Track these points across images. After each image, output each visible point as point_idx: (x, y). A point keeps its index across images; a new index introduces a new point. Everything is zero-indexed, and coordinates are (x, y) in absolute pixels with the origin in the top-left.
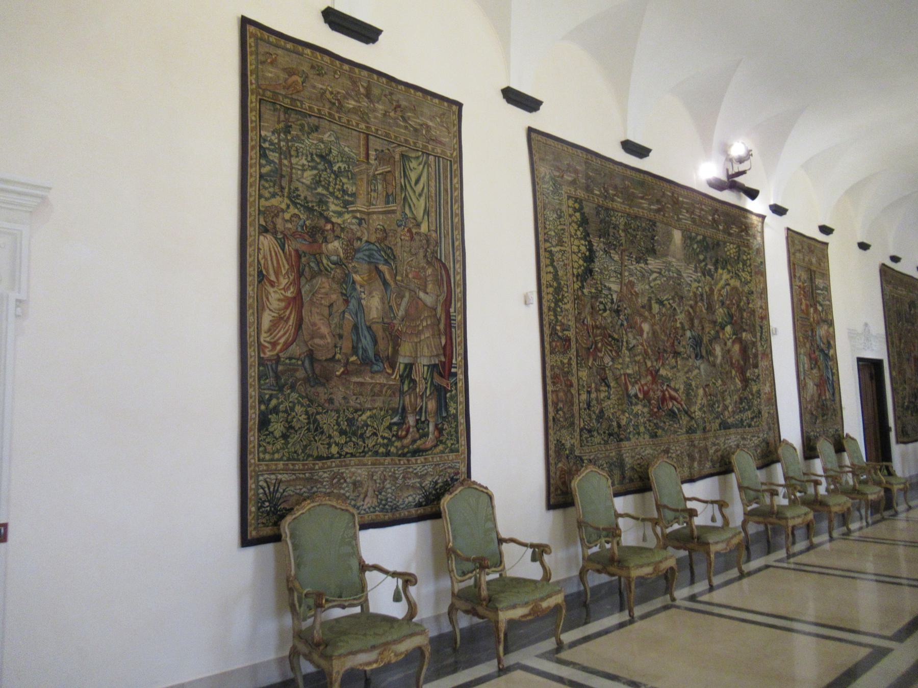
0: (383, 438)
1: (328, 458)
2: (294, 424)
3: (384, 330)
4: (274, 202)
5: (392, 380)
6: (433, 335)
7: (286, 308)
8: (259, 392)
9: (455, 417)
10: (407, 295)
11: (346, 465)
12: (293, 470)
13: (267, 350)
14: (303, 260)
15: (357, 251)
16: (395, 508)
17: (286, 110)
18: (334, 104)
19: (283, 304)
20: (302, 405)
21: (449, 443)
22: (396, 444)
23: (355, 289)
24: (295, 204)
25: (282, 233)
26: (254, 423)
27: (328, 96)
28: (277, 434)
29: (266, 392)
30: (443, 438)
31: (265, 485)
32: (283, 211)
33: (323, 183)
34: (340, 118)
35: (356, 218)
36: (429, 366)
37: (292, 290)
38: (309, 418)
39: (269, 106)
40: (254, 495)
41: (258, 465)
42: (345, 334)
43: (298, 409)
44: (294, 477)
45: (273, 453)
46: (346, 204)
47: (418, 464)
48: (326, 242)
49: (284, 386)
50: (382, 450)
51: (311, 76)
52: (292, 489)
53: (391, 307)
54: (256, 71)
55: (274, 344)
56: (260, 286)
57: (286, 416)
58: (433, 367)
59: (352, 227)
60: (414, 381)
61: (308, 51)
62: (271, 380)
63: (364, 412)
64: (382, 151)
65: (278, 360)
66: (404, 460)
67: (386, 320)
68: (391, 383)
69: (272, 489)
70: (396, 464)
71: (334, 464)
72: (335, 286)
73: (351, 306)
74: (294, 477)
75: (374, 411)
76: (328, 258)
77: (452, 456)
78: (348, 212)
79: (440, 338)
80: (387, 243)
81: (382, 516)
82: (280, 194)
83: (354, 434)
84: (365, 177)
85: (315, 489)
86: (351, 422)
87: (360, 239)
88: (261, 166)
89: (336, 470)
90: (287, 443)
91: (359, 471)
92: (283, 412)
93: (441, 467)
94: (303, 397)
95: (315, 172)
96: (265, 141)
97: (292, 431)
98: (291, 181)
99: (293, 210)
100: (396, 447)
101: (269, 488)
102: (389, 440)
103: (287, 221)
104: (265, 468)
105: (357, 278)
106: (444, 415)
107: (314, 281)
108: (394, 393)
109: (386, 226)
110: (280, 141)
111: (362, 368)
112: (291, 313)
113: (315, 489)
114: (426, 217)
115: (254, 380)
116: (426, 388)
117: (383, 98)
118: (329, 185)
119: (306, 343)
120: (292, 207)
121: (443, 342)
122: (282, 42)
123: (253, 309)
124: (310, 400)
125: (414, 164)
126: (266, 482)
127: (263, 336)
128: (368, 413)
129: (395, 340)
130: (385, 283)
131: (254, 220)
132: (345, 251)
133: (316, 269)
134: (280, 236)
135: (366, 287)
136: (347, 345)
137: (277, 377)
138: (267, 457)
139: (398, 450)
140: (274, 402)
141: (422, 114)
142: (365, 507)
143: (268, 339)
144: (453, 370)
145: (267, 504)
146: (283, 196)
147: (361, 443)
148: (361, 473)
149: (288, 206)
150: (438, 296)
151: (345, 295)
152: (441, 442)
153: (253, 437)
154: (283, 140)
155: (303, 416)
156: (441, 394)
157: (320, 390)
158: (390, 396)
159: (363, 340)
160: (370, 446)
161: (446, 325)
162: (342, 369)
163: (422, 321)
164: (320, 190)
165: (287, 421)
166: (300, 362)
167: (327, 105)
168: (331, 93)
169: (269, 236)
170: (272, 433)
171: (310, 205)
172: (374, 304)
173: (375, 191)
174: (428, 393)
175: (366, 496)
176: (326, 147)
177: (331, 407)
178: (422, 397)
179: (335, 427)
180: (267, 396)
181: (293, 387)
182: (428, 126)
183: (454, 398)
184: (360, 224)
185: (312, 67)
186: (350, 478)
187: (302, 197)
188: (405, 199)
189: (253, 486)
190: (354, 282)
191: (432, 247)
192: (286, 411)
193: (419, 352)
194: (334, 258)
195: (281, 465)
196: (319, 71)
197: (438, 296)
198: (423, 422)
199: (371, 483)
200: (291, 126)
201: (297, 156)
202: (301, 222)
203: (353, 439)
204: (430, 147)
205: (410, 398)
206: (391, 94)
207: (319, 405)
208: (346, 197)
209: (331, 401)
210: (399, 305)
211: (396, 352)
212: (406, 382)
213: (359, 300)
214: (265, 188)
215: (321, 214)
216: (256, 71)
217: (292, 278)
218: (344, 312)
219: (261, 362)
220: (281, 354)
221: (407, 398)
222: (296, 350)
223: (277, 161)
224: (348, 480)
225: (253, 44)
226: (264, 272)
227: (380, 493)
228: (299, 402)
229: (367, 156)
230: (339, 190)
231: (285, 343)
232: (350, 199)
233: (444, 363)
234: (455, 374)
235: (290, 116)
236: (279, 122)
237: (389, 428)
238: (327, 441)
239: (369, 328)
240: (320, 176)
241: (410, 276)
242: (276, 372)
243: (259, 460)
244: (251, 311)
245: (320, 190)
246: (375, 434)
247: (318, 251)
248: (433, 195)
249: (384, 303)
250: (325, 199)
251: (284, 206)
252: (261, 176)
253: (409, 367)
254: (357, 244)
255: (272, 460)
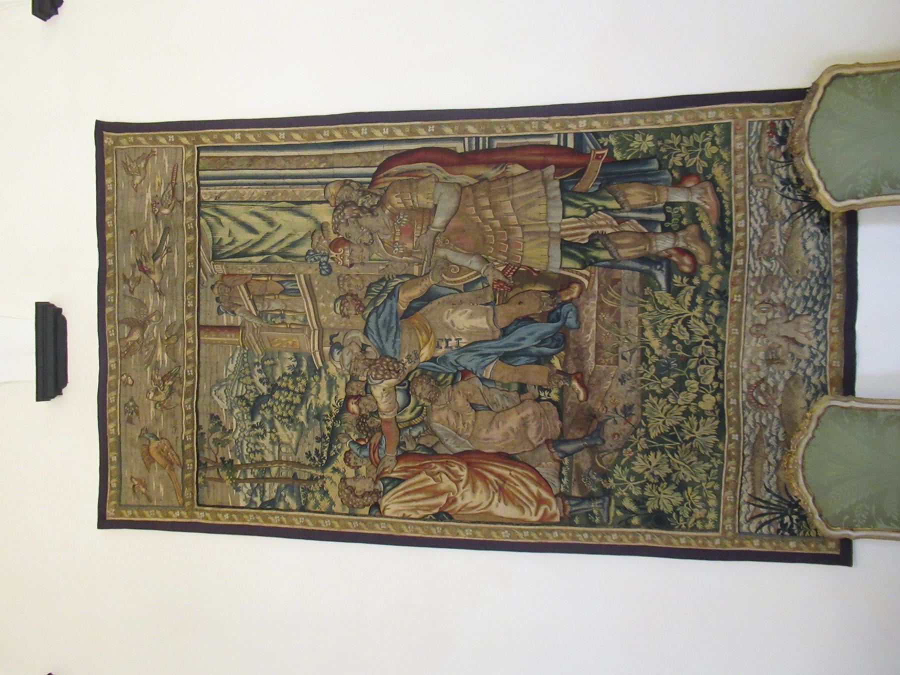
0: (693, 305)
1: (721, 416)
2: (662, 475)
3: (506, 301)
4: (333, 492)
5: (591, 286)
6: (509, 192)
7: (484, 479)
8: (613, 526)
9: (661, 135)
10: (442, 252)
11: (736, 378)
12: (737, 475)
13: (550, 512)
14: (410, 447)
15: (383, 354)
16: (824, 280)
17: (202, 465)
18: (171, 387)
19: (479, 484)
20: (633, 458)
21: (710, 150)
22: (705, 276)
23: (444, 359)
24: (331, 459)
25: (375, 483)
26: (659, 535)
27: (162, 397)
28: (677, 499)
29: (612, 515)
30: (702, 165)
31: (755, 523)
32: (344, 479)
33: (291, 413)
34: (188, 378)
35: (331, 353)
36: (565, 203)
37: (456, 468)
38: (655, 450)
39: (204, 491)
40: (770, 541)
41: (725, 532)
42: (517, 377)
43: (639, 466)
44: (748, 474)
45: (708, 508)
46: (314, 371)
47: (747, 225)
48: (377, 412)
49: (604, 489)
50: (714, 310)
51: (143, 425)
52: (767, 477)
53: (468, 287)
54: (165, 509)
55: (540, 501)
56: (455, 517)
57: (649, 486)
58: (568, 195)
59: (346, 362)
60: (593, 238)
61: (110, 427)
62: (595, 506)
63: (646, 345)
64: (217, 299)
65: (563, 496)
66: (737, 259)
67: (490, 299)
68: (596, 287)
69: (764, 511)
70: (743, 274)
71: (733, 366)
72: (443, 398)
73: (471, 366)
74: (748, 474)
75: (646, 322)
76: (401, 410)
77: (737, 142)
78: (326, 367)
79: (513, 177)
80: (361, 295)
81: (836, 307)
82: (320, 482)
83: (683, 363)
84: (265, 333)
85: (772, 441)
86: (662, 370)
87: (363, 348)
88: (288, 509)
89: (742, 398)
90: (693, 484)
91: (748, 352)
92: (643, 490)
93: (756, 170)
94: (621, 457)
95: (277, 423)
96: (251, 501)
97: (674, 476)
98: (299, 464)
99: (339, 463)
100: (711, 275)
101: (762, 515)
102: (696, 292)
103: (357, 474)
104: (729, 520)
105: (425, 354)
106: (655, 165)
107: (439, 432)
108: (616, 281)
109: (335, 296)
110: (246, 480)
111: (572, 346)
112: (492, 472)
113: (772, 441)
114: (306, 208)
115: (595, 533)
116: (606, 210)
117: (136, 295)
118: (291, 403)
119: (536, 449)
120: (335, 465)
121: (517, 169)
122: (112, 468)
123: (490, 529)
124: (626, 446)
125: (222, 234)
126: (753, 518)
127: (529, 516)
128: (649, 334)
129: (522, 276)
130: (428, 297)
131: (365, 522)
132: (388, 374)
133: (420, 429)
134: (380, 486)
135: (439, 336)
136: (536, 375)
137: (590, 497)
138: (712, 515)
139: (717, 272)
140: (628, 504)
141: (139, 215)
142: (813, 343)
143: (533, 509)
144: (571, 144)
145: (787, 519)
146: (322, 477)
147: (700, 350)
148: (752, 349)
149: (336, 470)
150: (437, 181)
151: (455, 375)
152: (707, 171)
153: (681, 539)
154: (245, 472)
155: (651, 457)
156: (620, 172)
157: (609, 429)
158: (619, 291)
159: (525, 344)
160: (705, 331)
161: (488, 164)
162: (575, 384)
163: (485, 220)
164: (302, 418)
165: (658, 484)
166: (566, 461)
167: (175, 399)
168: (156, 392)
169: (383, 503)
170: (675, 508)
171: (327, 432)
172: (466, 321)
173: (283, 316)
174: (612, 204)
175: (794, 341)
176: (237, 406)
177: (636, 411)
178: (621, 221)
179: (671, 398)
180: (619, 513)
181: (605, 475)
182: (155, 203)
183: (625, 138)
184: (340, 347)
185: (130, 421)
186: (758, 369)
187: (318, 446)
188: (283, 254)
189: (756, 542)
190: (433, 359)
191: (354, 196)
192: (643, 486)
193: (540, 221)
194: (400, 397)
195: (726, 495)
196: (132, 412)
197: (437, 181)
198: (669, 218)
199: (773, 328)
200: (223, 459)
201: (262, 452)
202: (354, 448)
203: (692, 366)
204: (189, 199)
205: (622, 246)
206: (126, 281)
207: (635, 433)
208: (304, 369)
209: (627, 411)
210: (462, 269)
211: (541, 277)
212: (595, 253)
213: (462, 350)
214: (317, 504)
215: (338, 418)
216: (165, 509)
217: (439, 468)
218: (482, 380)
219: (568, 520)
220: (555, 492)
221: (624, 253)
222: (547, 469)
223: (276, 486)
224: (762, 374)
225: (130, 512)
226: (436, 511)
227: (793, 310)
228: (629, 464)
229: (231, 328)
230: (295, 383)
231: (538, 484)
232: (305, 363)
233: (557, 166)
234: (578, 137)
235: (208, 460)
236: (221, 480)
237: (674, 291)
238: (693, 419)
239: (505, 332)
240: (282, 416)
241: (409, 246)
242: (582, 499)
243: (717, 530)
244: (494, 533)
245: (302, 418)
246: (685, 322)
247: (393, 425)
248: (265, 191)
249: (461, 302)
250: (313, 411)
251: (337, 478)
252: (302, 509)
253: (567, 248)
254: (372, 353)
255: (718, 509)
